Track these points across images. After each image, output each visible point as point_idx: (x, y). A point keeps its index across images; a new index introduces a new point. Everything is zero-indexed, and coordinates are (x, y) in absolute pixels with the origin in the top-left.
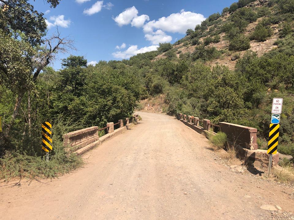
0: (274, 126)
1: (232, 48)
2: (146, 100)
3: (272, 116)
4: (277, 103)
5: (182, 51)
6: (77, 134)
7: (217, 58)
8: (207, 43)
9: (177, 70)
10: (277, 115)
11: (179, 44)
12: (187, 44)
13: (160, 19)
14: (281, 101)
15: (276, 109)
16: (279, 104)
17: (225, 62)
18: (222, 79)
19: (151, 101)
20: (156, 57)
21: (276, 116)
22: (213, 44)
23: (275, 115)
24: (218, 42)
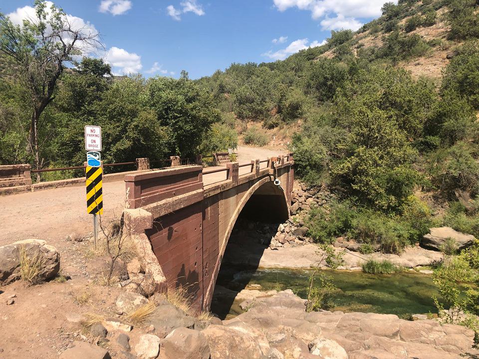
0: (93, 170)
1: (453, 36)
2: (276, 129)
3: (88, 155)
4: (93, 133)
5: (365, 44)
6: (190, 179)
7: (420, 56)
8: (410, 27)
9: (332, 79)
10: (94, 153)
11: (365, 31)
12: (376, 32)
13: (19, 10)
14: (98, 130)
15: (93, 144)
16: (96, 136)
17: (433, 62)
18: (384, 94)
19: (282, 131)
20: (322, 55)
21: (94, 155)
22: (422, 29)
23: (92, 153)
24: (432, 24)
